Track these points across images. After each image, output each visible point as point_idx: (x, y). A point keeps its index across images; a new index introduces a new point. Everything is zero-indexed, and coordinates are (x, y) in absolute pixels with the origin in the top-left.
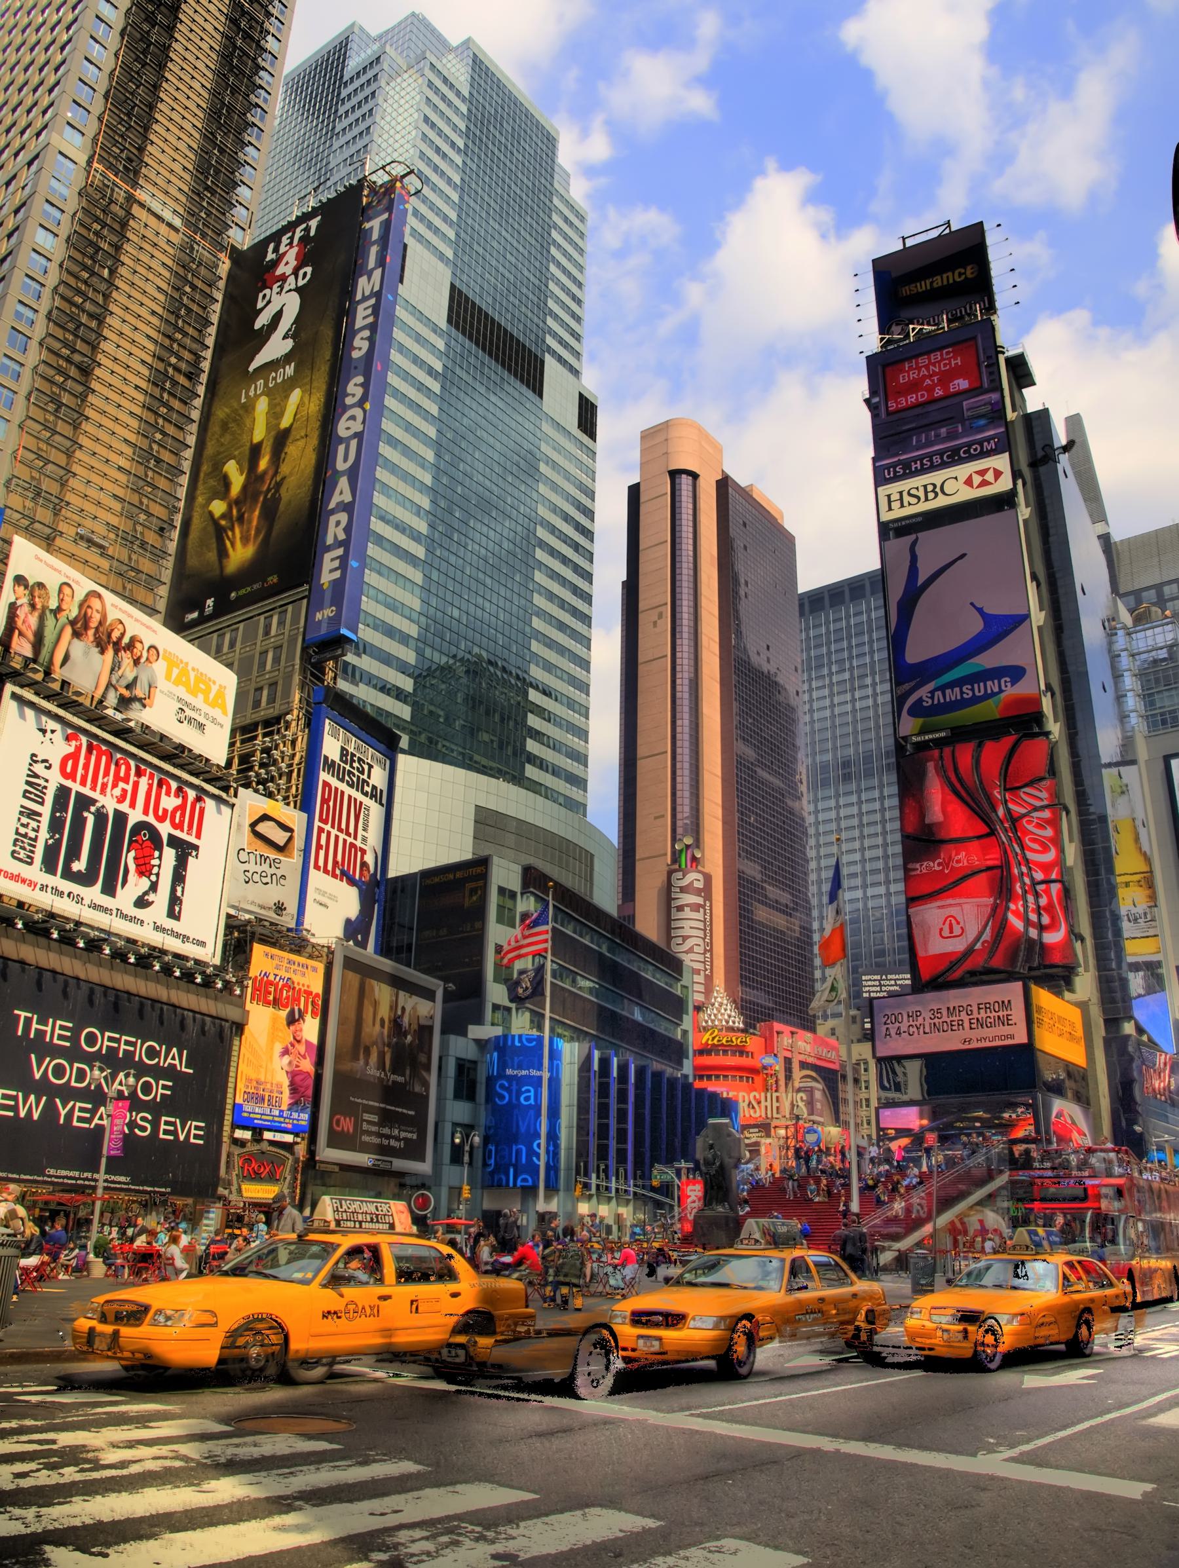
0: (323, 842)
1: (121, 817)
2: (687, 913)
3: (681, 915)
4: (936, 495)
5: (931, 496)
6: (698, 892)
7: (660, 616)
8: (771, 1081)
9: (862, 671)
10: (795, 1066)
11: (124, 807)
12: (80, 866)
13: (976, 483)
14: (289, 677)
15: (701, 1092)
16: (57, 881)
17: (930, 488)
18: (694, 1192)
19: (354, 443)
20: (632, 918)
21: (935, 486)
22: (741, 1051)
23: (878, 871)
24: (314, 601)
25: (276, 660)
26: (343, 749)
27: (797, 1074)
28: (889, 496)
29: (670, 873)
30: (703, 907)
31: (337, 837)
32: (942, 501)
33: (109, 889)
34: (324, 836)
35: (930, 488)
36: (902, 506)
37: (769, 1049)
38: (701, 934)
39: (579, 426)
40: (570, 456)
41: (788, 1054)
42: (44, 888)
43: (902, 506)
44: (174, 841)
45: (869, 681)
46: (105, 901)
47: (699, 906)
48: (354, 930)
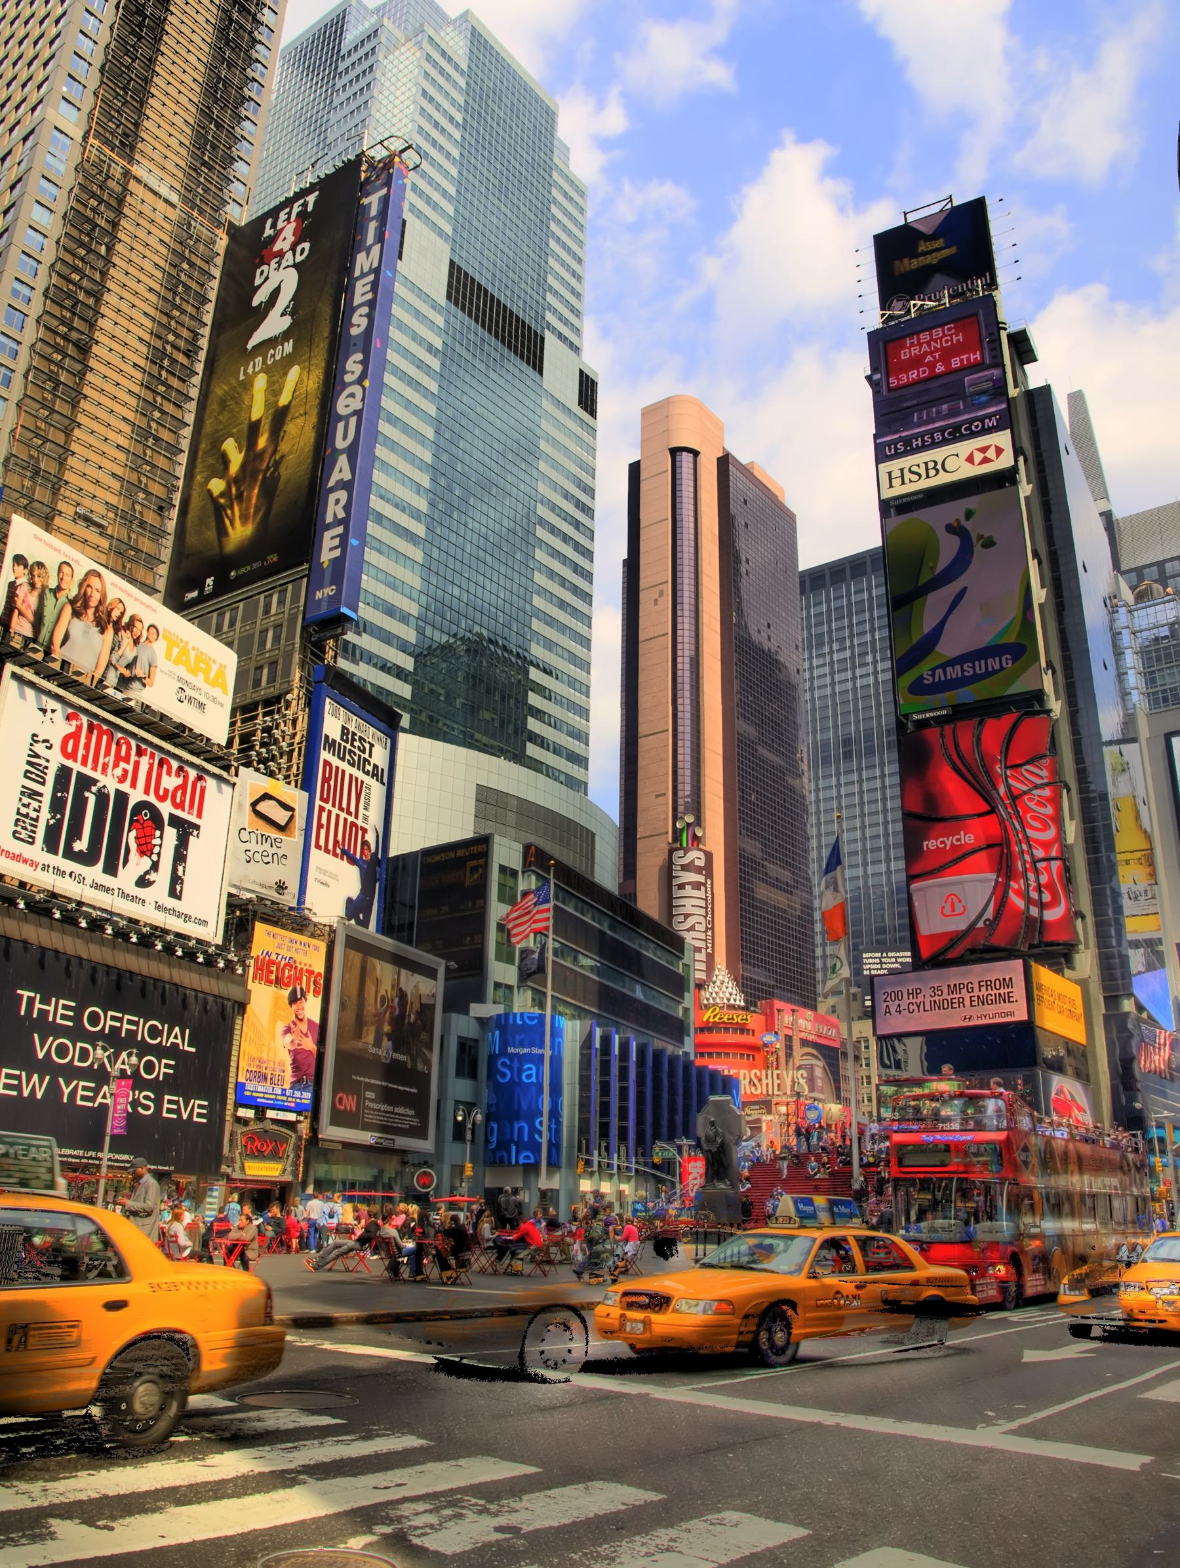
0: (324, 821)
1: (122, 797)
2: (688, 891)
3: (682, 893)
5: (932, 473)
6: (699, 870)
7: (661, 594)
9: (863, 649)
10: (796, 1044)
11: (125, 787)
12: (81, 845)
14: (289, 657)
15: (701, 1071)
16: (58, 861)
17: (931, 465)
18: (696, 1169)
19: (353, 421)
20: (633, 897)
22: (742, 1029)
24: (315, 582)
25: (276, 639)
26: (343, 728)
27: (798, 1051)
29: (671, 852)
30: (705, 885)
31: (338, 816)
32: (942, 479)
33: (111, 869)
34: (325, 815)
35: (931, 465)
37: (770, 1027)
38: (703, 912)
41: (789, 1032)
42: (45, 868)
44: (175, 821)
45: (869, 658)
46: (107, 880)
48: (356, 909)
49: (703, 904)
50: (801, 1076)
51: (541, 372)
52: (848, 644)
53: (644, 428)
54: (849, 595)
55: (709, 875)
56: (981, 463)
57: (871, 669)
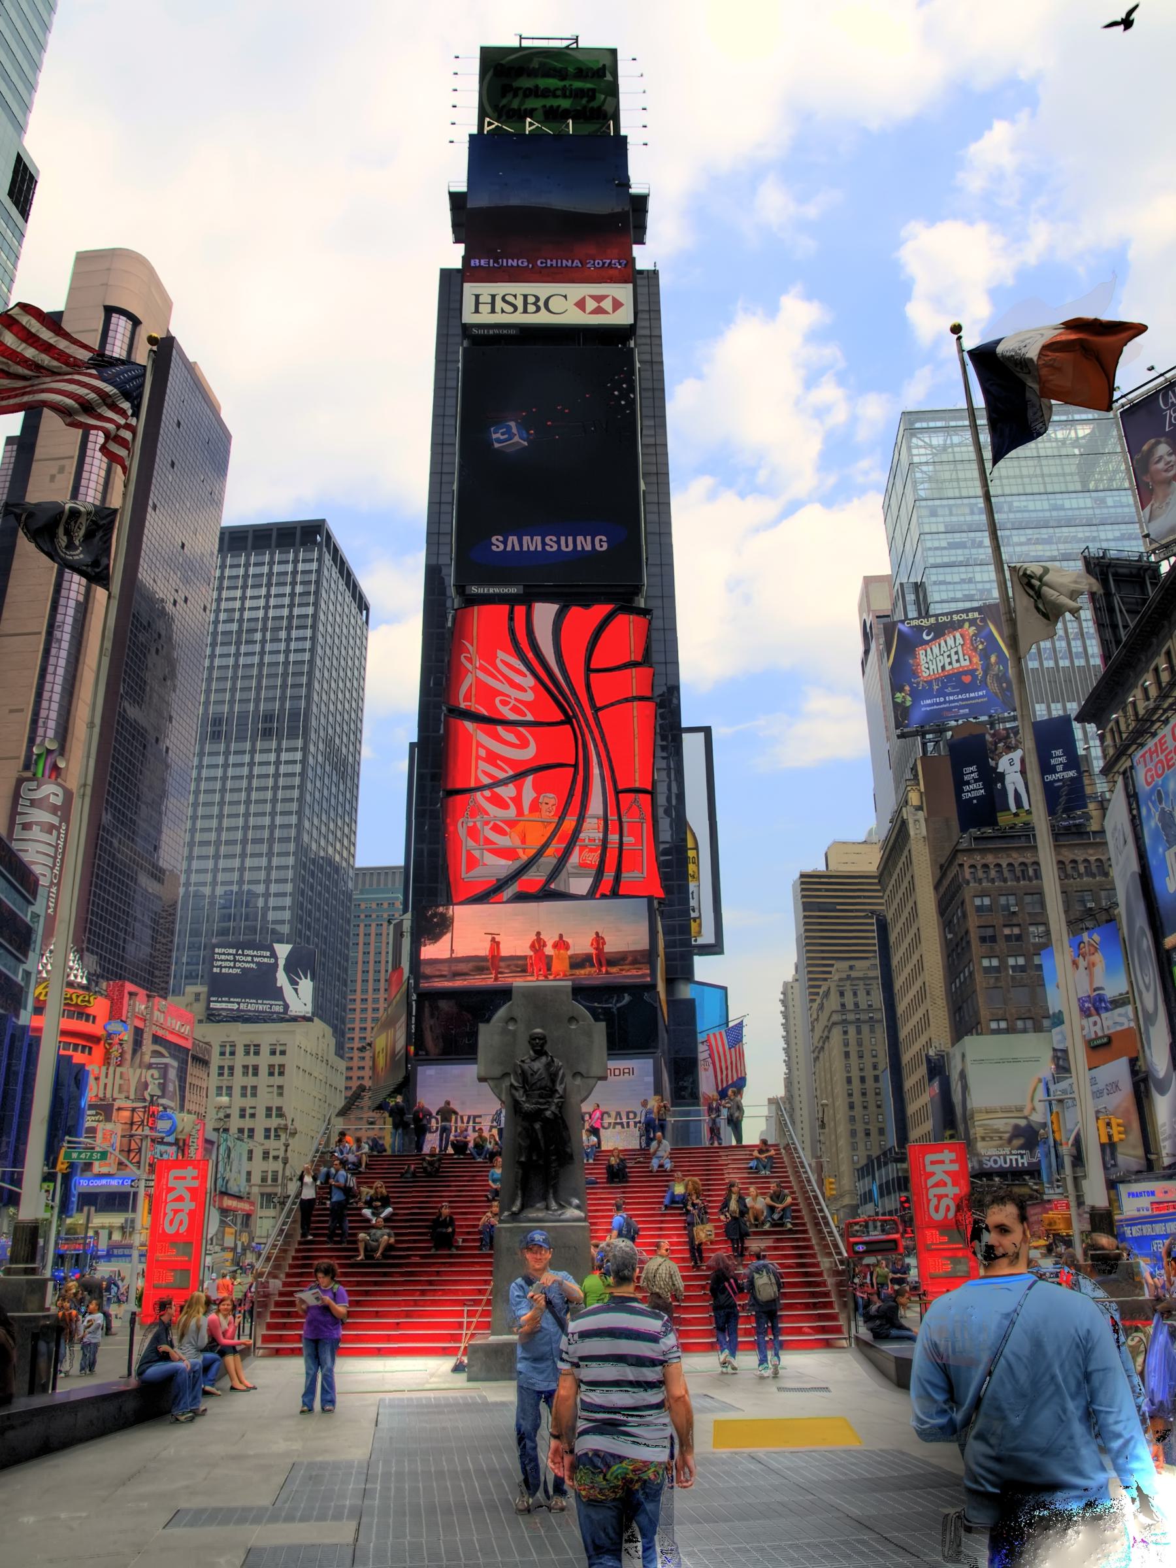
2: (36, 833)
4: (538, 309)
5: (531, 308)
6: (54, 809)
7: (62, 470)
8: (115, 1051)
9: (252, 625)
17: (531, 300)
27: (148, 1046)
28: (477, 297)
29: (20, 782)
30: (58, 828)
36: (493, 311)
39: (11, 194)
41: (140, 1024)
43: (493, 311)
45: (258, 636)
49: (51, 851)
50: (152, 1077)
52: (237, 615)
53: (76, 275)
55: (66, 818)
56: (592, 313)
57: (257, 648)
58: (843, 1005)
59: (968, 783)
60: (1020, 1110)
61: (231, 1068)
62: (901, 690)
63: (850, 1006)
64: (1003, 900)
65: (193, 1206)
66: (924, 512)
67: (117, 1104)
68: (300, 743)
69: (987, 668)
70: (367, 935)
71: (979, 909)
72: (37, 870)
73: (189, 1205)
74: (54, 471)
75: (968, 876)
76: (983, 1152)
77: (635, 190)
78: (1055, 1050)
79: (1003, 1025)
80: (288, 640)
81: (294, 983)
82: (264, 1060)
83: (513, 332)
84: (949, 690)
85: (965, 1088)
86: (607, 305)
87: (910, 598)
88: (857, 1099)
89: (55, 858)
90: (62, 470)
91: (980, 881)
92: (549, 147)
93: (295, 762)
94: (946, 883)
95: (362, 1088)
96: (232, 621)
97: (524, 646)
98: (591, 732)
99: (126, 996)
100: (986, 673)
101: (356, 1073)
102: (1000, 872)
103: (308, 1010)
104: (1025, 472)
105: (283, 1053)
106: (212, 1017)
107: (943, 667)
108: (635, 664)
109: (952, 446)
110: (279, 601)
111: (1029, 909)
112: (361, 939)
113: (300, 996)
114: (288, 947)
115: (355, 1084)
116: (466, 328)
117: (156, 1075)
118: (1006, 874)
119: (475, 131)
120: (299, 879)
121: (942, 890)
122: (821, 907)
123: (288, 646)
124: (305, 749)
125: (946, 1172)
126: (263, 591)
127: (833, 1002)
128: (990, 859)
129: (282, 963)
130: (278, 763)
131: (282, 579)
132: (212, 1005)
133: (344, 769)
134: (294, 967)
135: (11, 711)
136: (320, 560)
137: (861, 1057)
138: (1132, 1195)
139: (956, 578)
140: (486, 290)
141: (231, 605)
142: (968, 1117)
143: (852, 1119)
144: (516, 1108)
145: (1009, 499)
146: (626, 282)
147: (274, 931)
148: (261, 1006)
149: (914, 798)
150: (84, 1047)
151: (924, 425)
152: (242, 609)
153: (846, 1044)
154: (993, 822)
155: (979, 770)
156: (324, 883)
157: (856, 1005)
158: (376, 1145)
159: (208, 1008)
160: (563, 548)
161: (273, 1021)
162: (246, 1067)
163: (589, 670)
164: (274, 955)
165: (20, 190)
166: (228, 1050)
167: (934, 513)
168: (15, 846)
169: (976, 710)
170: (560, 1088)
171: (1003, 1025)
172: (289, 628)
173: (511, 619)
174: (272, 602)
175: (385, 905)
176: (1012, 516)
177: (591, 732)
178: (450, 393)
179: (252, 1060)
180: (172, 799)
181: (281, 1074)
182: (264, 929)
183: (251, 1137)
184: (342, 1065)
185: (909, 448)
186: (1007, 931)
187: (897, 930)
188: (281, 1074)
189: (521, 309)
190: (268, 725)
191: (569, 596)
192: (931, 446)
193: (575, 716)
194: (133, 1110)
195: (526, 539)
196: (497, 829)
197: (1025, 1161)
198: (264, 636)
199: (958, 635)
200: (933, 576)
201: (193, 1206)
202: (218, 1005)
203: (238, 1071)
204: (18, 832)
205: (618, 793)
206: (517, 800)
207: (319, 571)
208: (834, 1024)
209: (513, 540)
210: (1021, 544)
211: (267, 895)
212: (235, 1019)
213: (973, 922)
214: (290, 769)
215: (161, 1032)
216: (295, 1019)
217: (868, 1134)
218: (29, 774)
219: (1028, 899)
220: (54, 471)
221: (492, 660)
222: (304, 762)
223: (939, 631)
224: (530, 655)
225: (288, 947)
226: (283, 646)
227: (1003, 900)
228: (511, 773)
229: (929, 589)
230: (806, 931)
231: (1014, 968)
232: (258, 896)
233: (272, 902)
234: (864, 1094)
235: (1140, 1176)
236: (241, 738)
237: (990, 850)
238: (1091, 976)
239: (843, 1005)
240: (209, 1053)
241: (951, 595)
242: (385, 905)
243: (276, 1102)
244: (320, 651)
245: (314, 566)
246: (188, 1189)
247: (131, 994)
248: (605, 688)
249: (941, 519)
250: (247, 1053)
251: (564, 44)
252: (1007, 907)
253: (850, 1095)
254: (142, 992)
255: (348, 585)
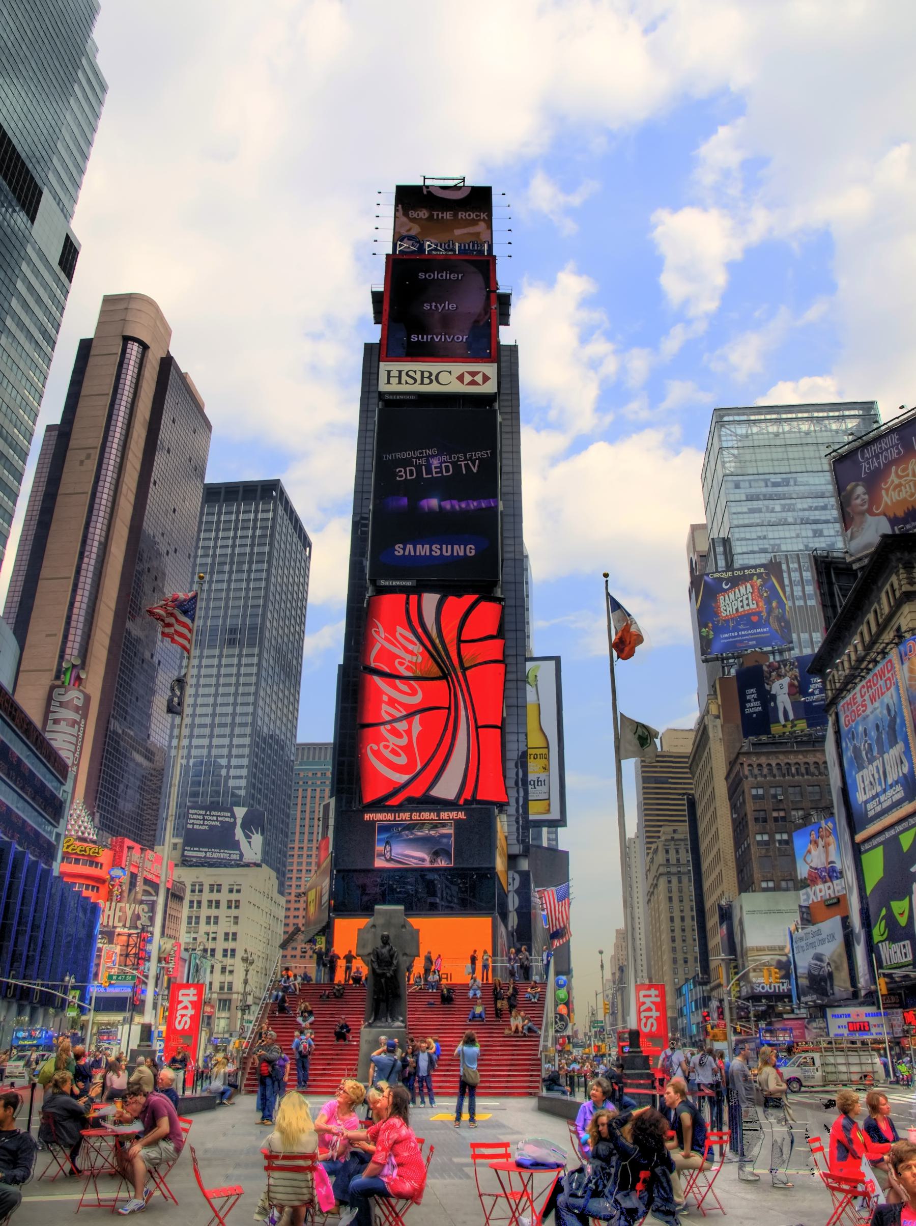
2: (63, 726)
3: (56, 728)
4: (431, 382)
5: (426, 381)
6: (77, 709)
8: (116, 892)
9: (223, 559)
10: (140, 881)
13: (480, 375)
17: (426, 374)
21: (431, 374)
23: (205, 726)
27: (140, 887)
28: (389, 372)
29: (52, 688)
30: (79, 723)
32: (434, 388)
35: (426, 374)
36: (400, 383)
38: (72, 748)
39: (60, 263)
40: (46, 285)
41: (134, 870)
43: (400, 383)
47: (75, 722)
49: (74, 740)
51: (33, 221)
52: (211, 552)
53: (103, 312)
54: (220, 514)
55: (85, 716)
57: (226, 577)
58: (668, 860)
59: (749, 701)
60: (782, 948)
61: (199, 902)
62: (706, 626)
63: (673, 861)
64: (772, 791)
65: (658, 1014)
66: (731, 485)
67: (118, 930)
68: (256, 651)
69: (770, 611)
70: (304, 797)
71: (756, 797)
72: (63, 754)
73: (655, 1014)
74: (83, 457)
75: (747, 772)
76: (754, 980)
77: (501, 290)
78: (800, 907)
79: (771, 884)
80: (250, 571)
81: (248, 837)
82: (224, 897)
83: (413, 397)
84: (742, 627)
85: (742, 932)
86: (479, 378)
87: (720, 549)
88: (678, 934)
89: (76, 745)
90: (88, 456)
91: (756, 777)
92: (440, 271)
93: (252, 665)
94: (732, 776)
95: (297, 930)
96: (207, 556)
97: (415, 623)
98: (460, 685)
99: (125, 849)
100: (769, 614)
101: (292, 913)
102: (771, 770)
103: (258, 858)
104: (807, 455)
105: (238, 891)
106: (185, 862)
107: (737, 609)
108: (492, 637)
109: (752, 434)
110: (243, 541)
111: (792, 798)
112: (300, 800)
113: (252, 847)
114: (245, 809)
115: (291, 929)
116: (381, 395)
117: (146, 909)
118: (775, 771)
119: (390, 252)
120: (254, 755)
121: (730, 781)
122: (657, 780)
123: (249, 576)
124: (260, 655)
125: (653, 1003)
126: (232, 534)
127: (660, 858)
128: (763, 760)
129: (239, 822)
130: (239, 665)
131: (246, 525)
132: (186, 853)
133: (289, 669)
134: (249, 824)
135: (48, 636)
136: (275, 511)
137: (681, 901)
138: (834, 1016)
139: (754, 536)
140: (394, 367)
141: (206, 543)
142: (744, 954)
143: (674, 950)
144: (373, 970)
145: (794, 475)
146: (492, 362)
147: (233, 795)
148: (223, 854)
149: (714, 709)
150: (93, 887)
151: (731, 418)
152: (215, 547)
153: (670, 891)
154: (767, 732)
155: (758, 692)
156: (272, 753)
157: (678, 860)
158: (306, 978)
159: (183, 855)
160: (444, 553)
161: (232, 866)
162: (210, 902)
163: (460, 641)
164: (233, 816)
165: (67, 259)
166: (197, 888)
167: (737, 486)
168: (48, 736)
169: (761, 642)
170: (395, 962)
171: (771, 884)
172: (251, 562)
173: (407, 603)
174: (238, 542)
175: (319, 775)
176: (796, 488)
177: (460, 685)
178: (369, 434)
179: (215, 896)
180: (157, 696)
181: (237, 907)
182: (226, 793)
183: (213, 955)
184: (282, 900)
185: (720, 436)
186: (775, 814)
187: (703, 804)
188: (237, 907)
189: (419, 381)
190: (232, 636)
191: (447, 588)
192: (736, 435)
193: (450, 674)
194: (129, 935)
195: (419, 547)
196: (394, 752)
197: (785, 987)
198: (231, 568)
199: (749, 585)
200: (737, 534)
201: (658, 1014)
202: (190, 854)
203: (205, 904)
204: (50, 726)
205: (477, 727)
206: (409, 732)
207: (274, 519)
208: (661, 874)
209: (410, 547)
210: (804, 510)
211: (229, 767)
212: (202, 865)
213: (750, 807)
214: (249, 670)
215: (150, 876)
216: (247, 865)
217: (686, 962)
218: (58, 683)
219: (791, 790)
220: (83, 457)
221: (393, 633)
222: (259, 665)
223: (735, 582)
224: (420, 630)
225: (245, 809)
226: (245, 576)
227: (772, 791)
228: (404, 713)
229: (733, 544)
230: (645, 799)
231: (780, 842)
232: (221, 767)
233: (233, 772)
234: (683, 930)
235: (849, 1002)
236: (212, 646)
237: (764, 753)
238: (827, 853)
239: (668, 860)
240: (184, 891)
241: (750, 548)
242: (319, 775)
243: (233, 929)
244: (273, 580)
245: (271, 515)
246: (653, 1003)
247: (129, 848)
248: (471, 654)
249: (742, 491)
250: (212, 891)
251: (455, 182)
252: (775, 796)
253: (673, 931)
254: (138, 847)
255: (295, 528)
